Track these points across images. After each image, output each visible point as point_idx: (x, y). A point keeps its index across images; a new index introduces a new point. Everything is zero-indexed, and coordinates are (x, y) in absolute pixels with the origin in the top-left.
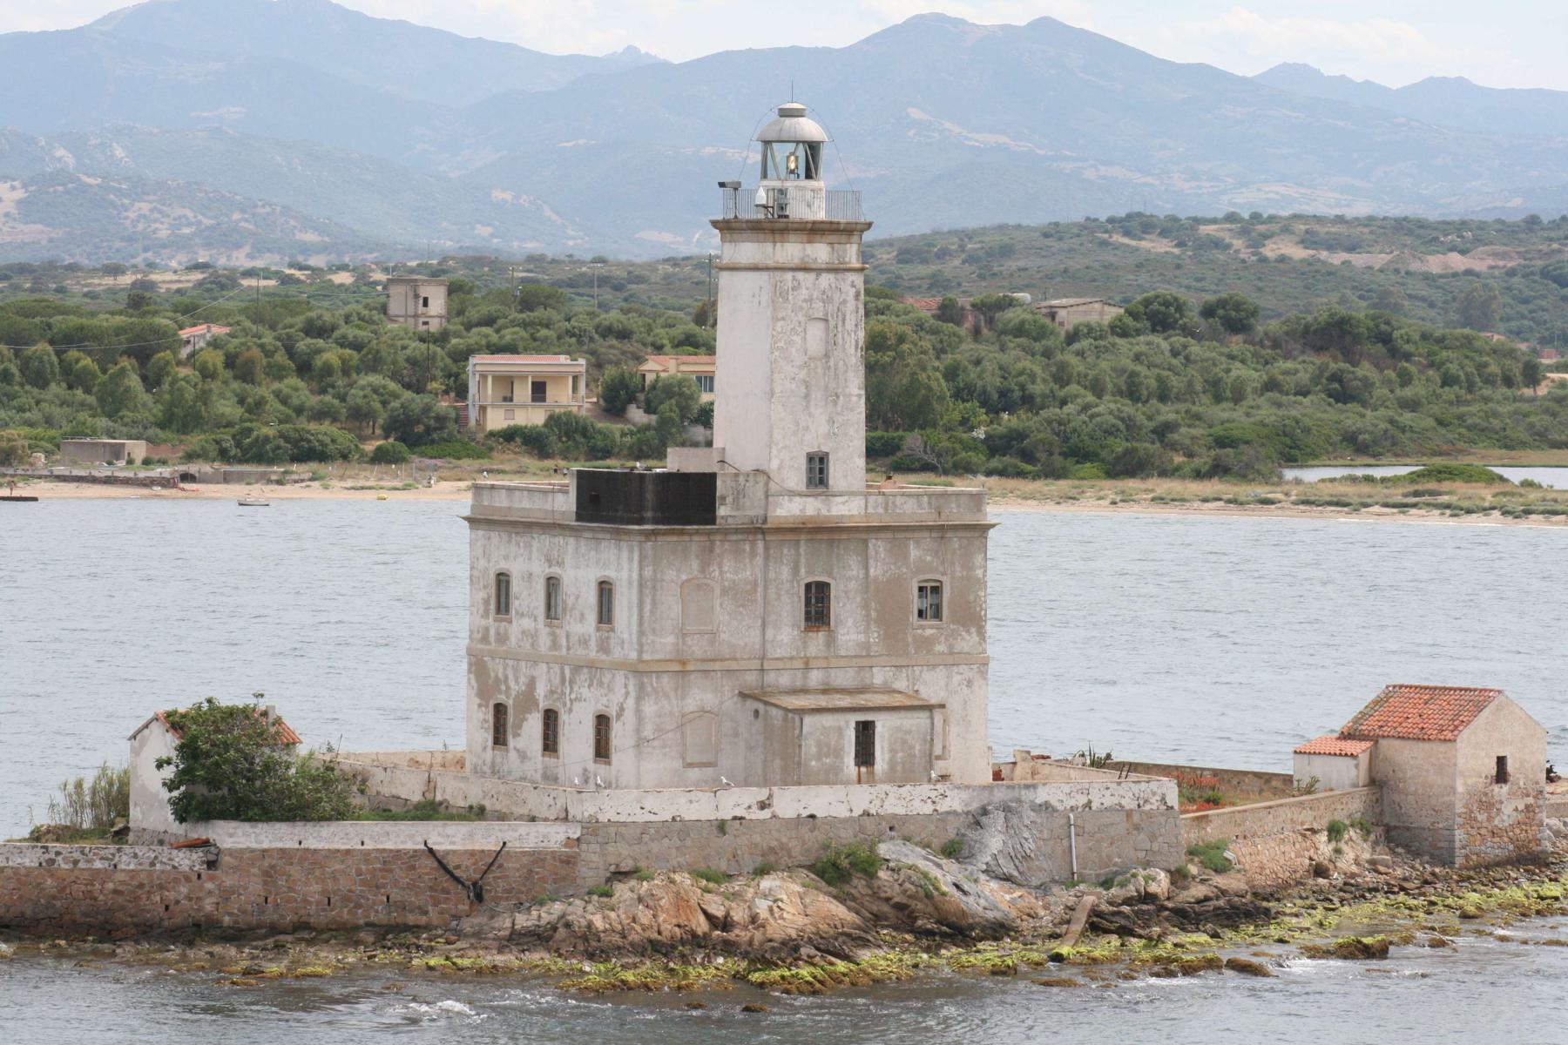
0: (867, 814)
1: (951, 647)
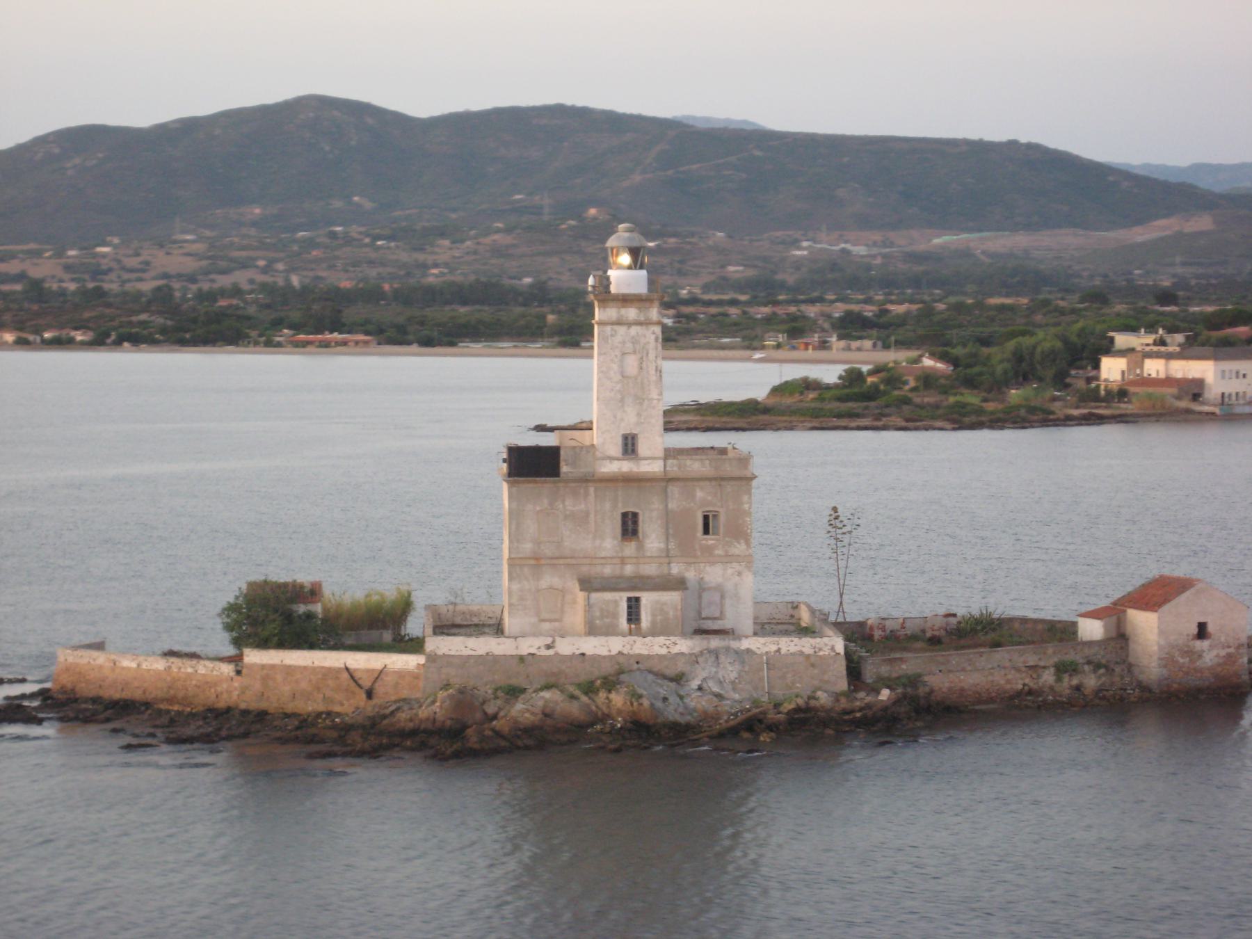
0: (620, 653)
1: (726, 551)
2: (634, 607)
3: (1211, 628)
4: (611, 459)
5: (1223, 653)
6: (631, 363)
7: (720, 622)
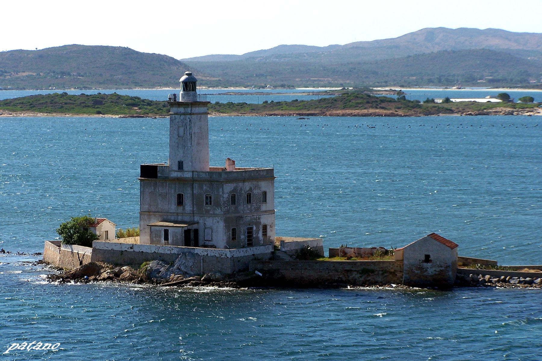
3: (432, 258)
5: (438, 269)
6: (181, 130)
7: (211, 242)
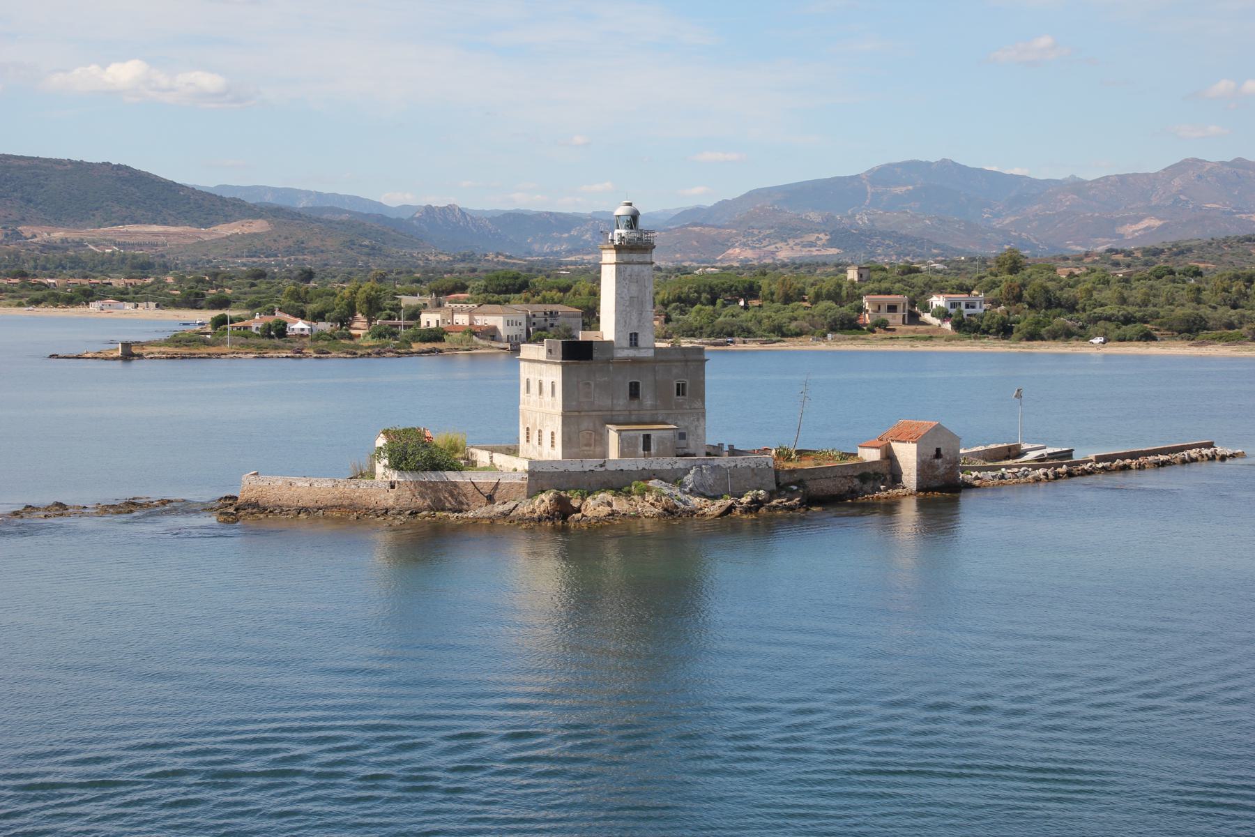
2: (647, 438)
4: (623, 348)
